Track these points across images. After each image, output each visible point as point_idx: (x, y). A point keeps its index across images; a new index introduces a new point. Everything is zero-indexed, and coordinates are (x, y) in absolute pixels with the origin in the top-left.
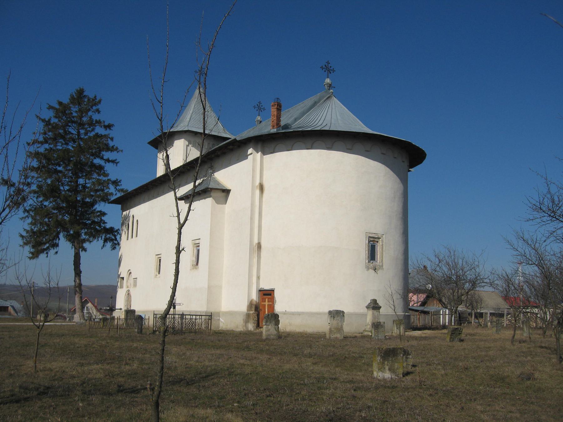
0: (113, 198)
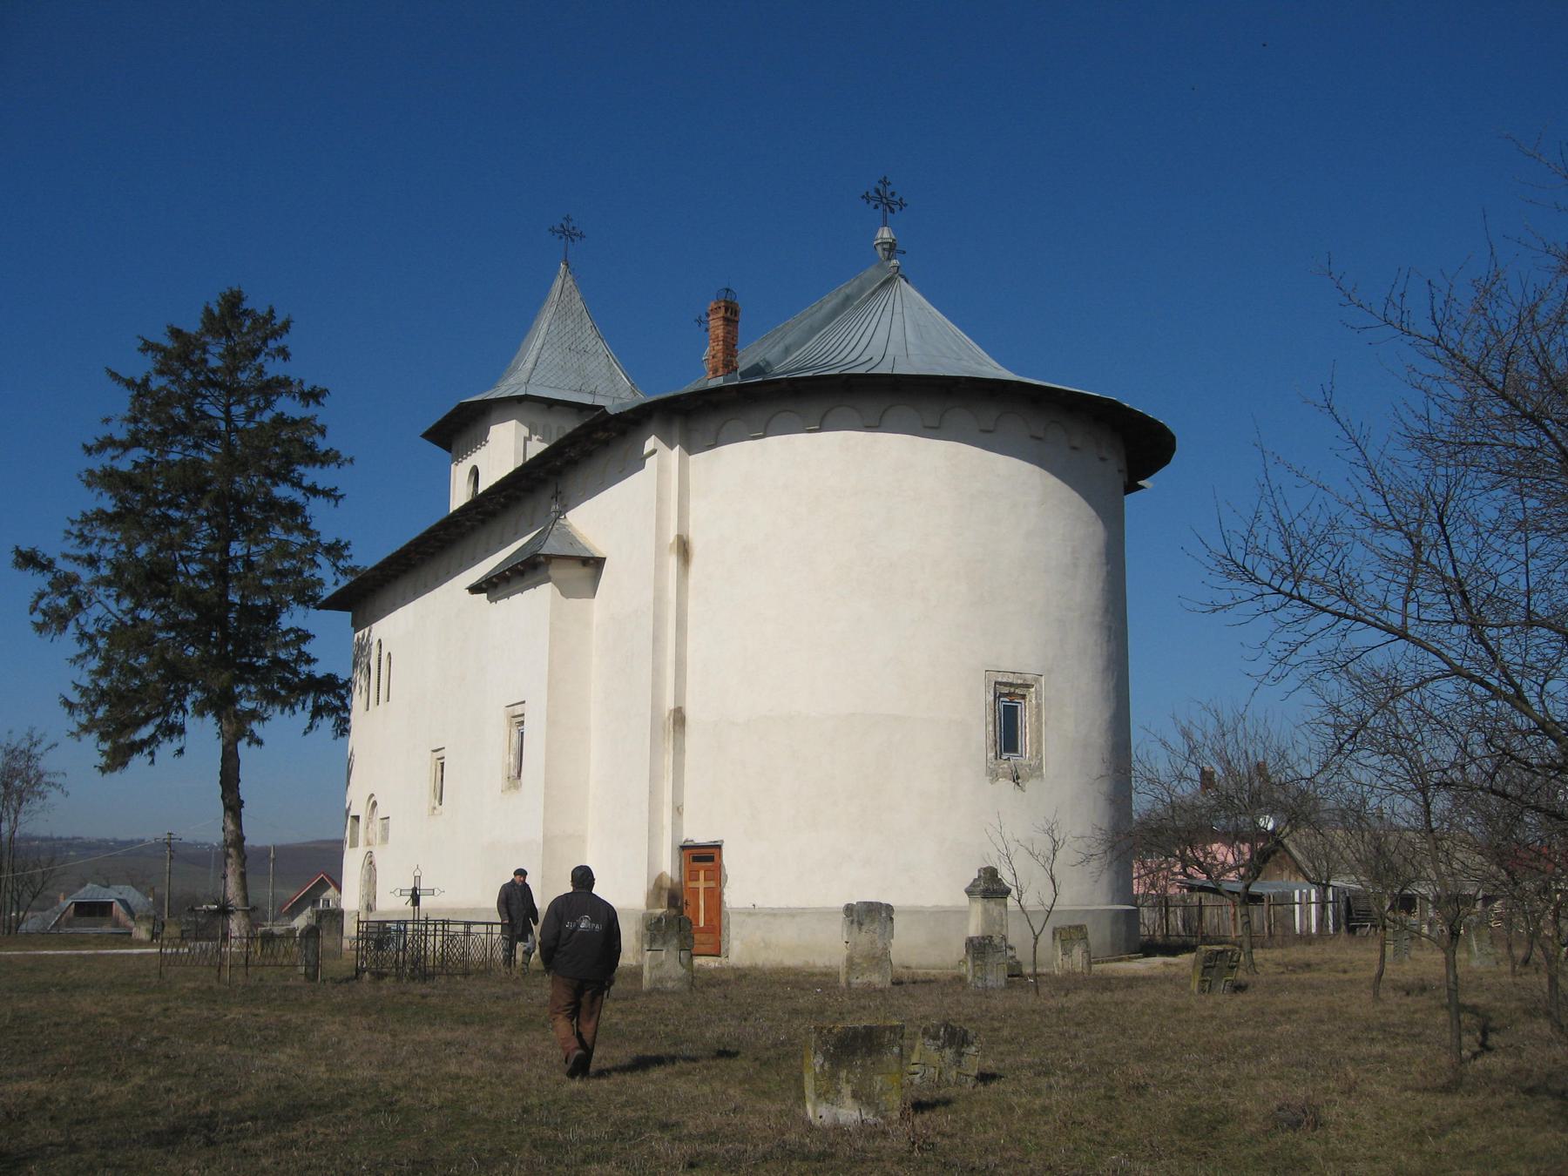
0: (328, 591)
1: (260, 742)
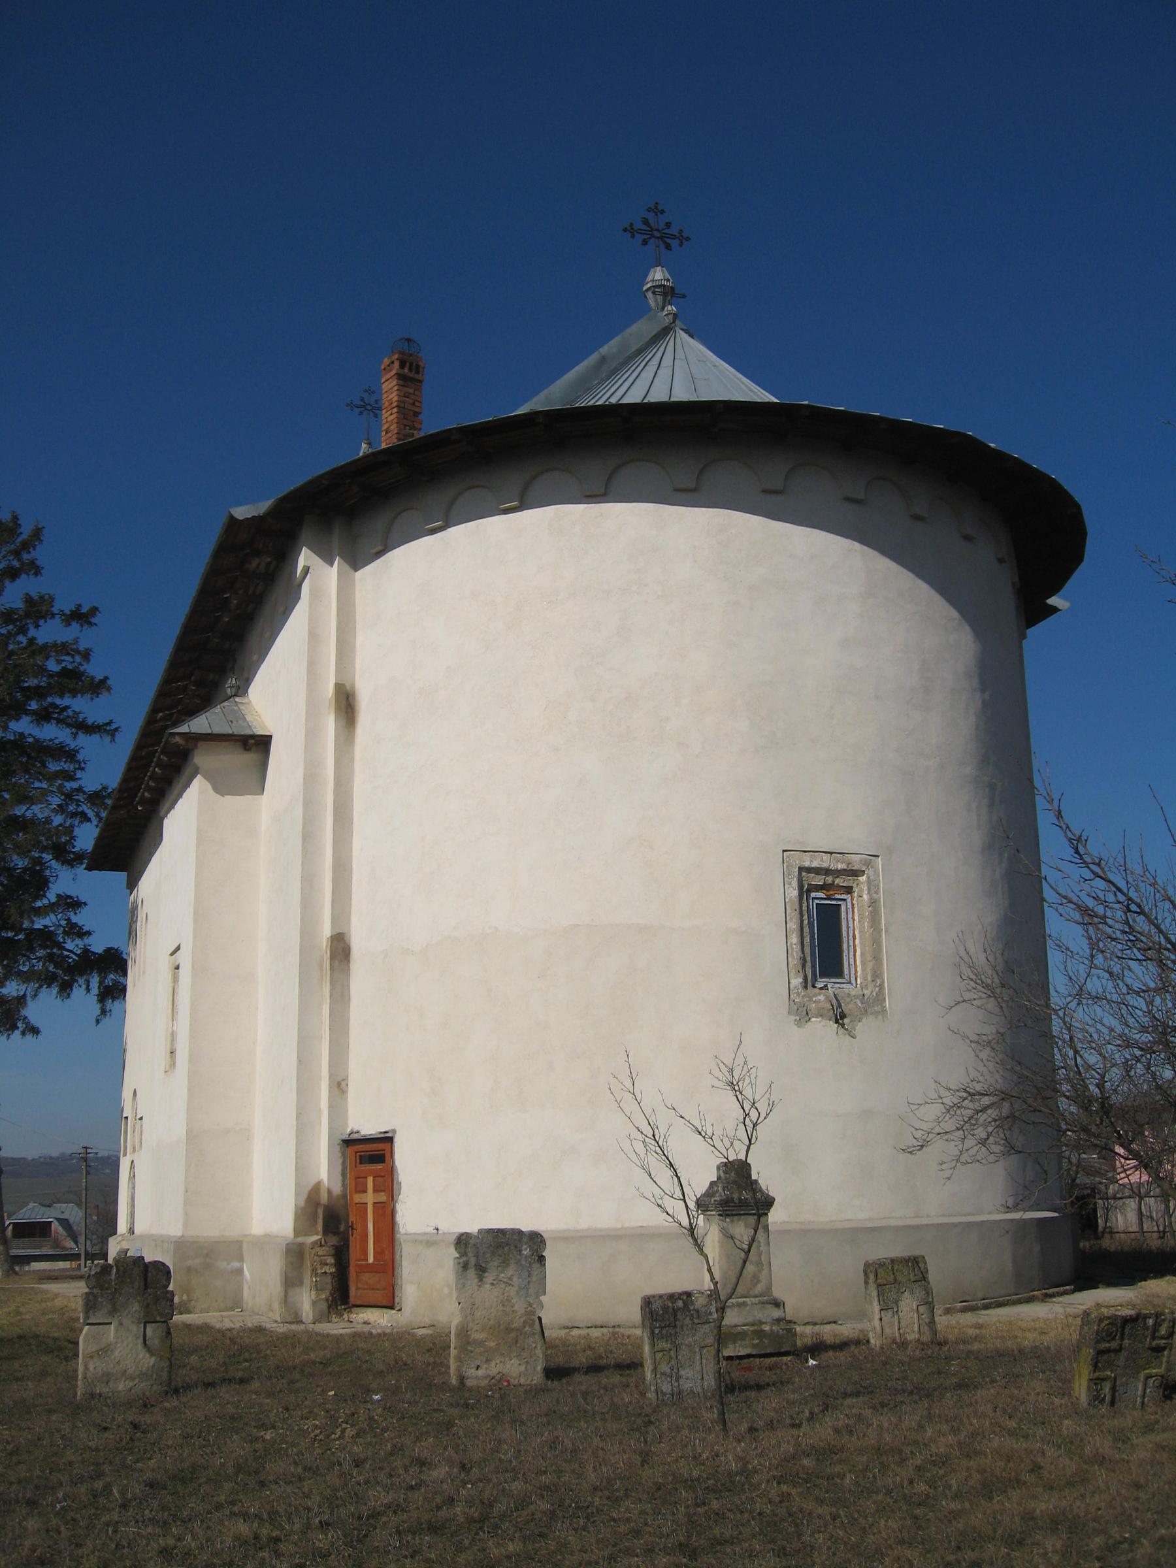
1: (35, 1031)
